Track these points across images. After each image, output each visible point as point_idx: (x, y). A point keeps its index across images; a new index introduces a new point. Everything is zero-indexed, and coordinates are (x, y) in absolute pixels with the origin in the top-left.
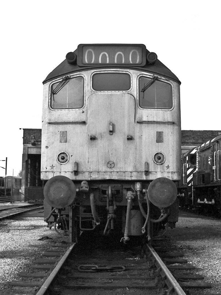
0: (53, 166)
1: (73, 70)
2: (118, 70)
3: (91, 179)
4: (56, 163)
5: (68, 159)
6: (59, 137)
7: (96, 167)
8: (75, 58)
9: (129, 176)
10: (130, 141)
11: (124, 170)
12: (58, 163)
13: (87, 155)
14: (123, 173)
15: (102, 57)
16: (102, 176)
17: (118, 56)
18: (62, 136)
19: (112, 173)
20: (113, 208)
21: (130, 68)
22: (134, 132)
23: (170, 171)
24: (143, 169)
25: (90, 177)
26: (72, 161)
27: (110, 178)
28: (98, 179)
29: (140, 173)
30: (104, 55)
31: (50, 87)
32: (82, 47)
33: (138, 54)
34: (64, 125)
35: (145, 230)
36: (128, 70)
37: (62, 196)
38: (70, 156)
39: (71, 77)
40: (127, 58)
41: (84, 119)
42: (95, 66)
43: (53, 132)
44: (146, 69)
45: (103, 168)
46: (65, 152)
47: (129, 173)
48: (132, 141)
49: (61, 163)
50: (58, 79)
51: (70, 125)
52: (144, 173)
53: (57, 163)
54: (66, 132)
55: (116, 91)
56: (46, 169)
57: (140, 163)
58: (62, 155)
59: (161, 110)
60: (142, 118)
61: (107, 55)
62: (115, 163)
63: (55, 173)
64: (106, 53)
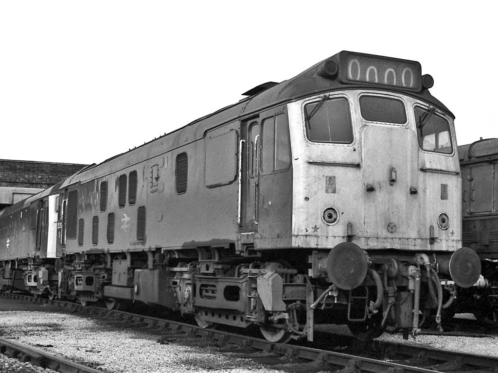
0: (317, 227)
1: (332, 88)
2: (390, 93)
3: (369, 248)
4: (320, 223)
5: (338, 218)
6: (325, 184)
7: (374, 231)
8: (336, 70)
9: (413, 244)
10: (413, 195)
11: (406, 236)
12: (324, 223)
13: (363, 214)
14: (406, 241)
15: (370, 73)
16: (382, 244)
17: (388, 75)
18: (329, 184)
19: (394, 239)
20: (394, 288)
21: (403, 92)
22: (417, 183)
23: (455, 239)
24: (427, 235)
25: (367, 245)
26: (342, 220)
27: (392, 247)
28: (377, 248)
29: (424, 241)
30: (372, 70)
31: (303, 108)
32: (345, 55)
33: (412, 74)
34: (331, 167)
35: (440, 319)
36: (401, 95)
37: (352, 271)
38: (341, 214)
39: (331, 97)
40: (381, 76)
41: (357, 162)
42: (352, 84)
43: (316, 177)
44: (419, 96)
45: (384, 233)
46: (334, 208)
47: (413, 240)
48: (415, 195)
49: (329, 224)
50: (314, 97)
51: (340, 168)
52: (428, 241)
53: (323, 224)
54: (335, 177)
55: (395, 124)
56: (307, 231)
57: (424, 225)
58: (331, 212)
59: (442, 154)
60: (424, 164)
61: (376, 71)
62: (397, 226)
63: (320, 237)
64: (375, 68)
